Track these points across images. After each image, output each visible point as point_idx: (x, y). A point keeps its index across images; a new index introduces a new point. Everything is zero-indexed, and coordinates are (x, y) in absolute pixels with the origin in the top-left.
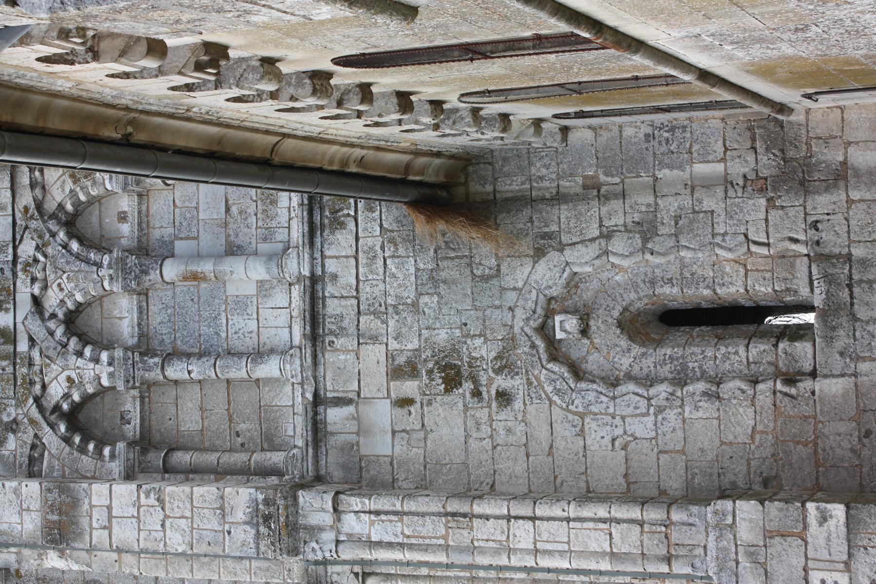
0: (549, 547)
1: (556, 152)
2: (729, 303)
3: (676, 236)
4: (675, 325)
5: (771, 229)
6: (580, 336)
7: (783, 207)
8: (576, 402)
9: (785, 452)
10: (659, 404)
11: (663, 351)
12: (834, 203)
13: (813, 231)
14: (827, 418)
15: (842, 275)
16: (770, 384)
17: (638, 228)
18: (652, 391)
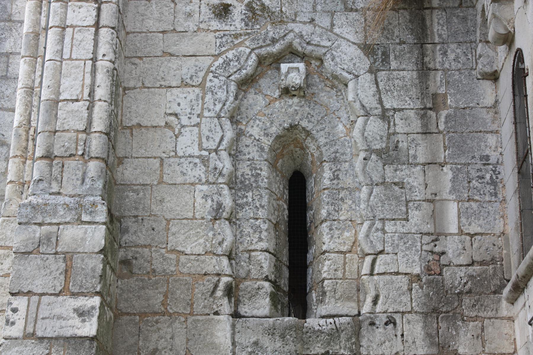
0: (67, 40)
1: (472, 69)
2: (311, 238)
3: (383, 183)
4: (290, 186)
5: (388, 277)
6: (283, 86)
7: (411, 290)
8: (216, 80)
9: (157, 283)
10: (211, 160)
11: (265, 168)
12: (414, 342)
13: (385, 320)
14: (190, 326)
15: (338, 347)
16: (228, 271)
17: (391, 146)
18: (224, 154)
